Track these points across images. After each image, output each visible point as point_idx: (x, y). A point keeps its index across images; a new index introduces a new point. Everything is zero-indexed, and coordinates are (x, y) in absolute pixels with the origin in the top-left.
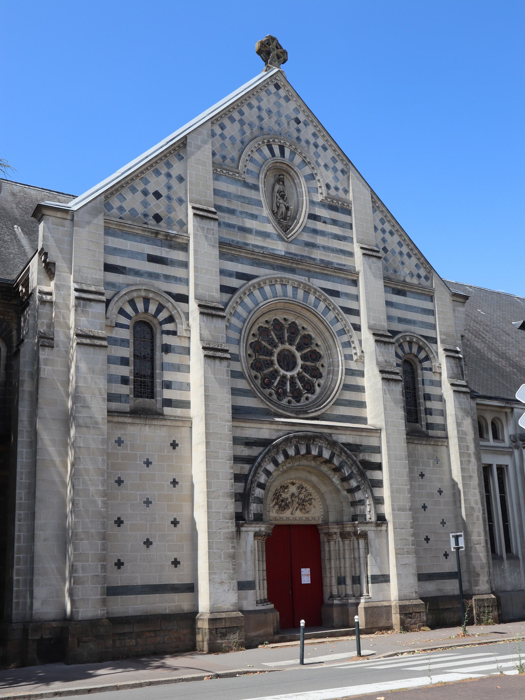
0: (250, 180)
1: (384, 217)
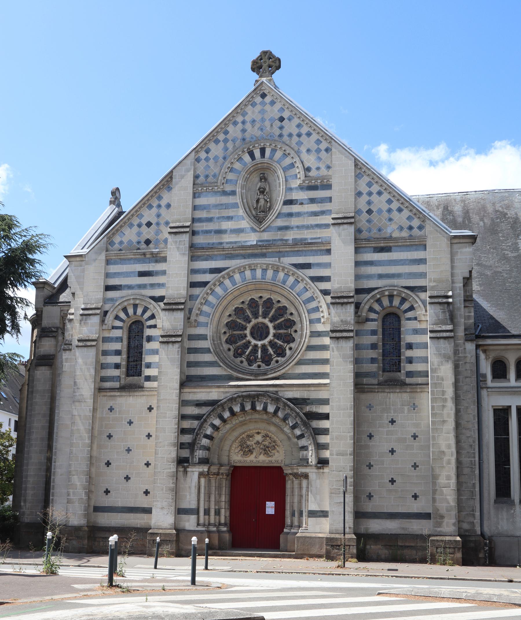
0: (228, 188)
1: (371, 180)
